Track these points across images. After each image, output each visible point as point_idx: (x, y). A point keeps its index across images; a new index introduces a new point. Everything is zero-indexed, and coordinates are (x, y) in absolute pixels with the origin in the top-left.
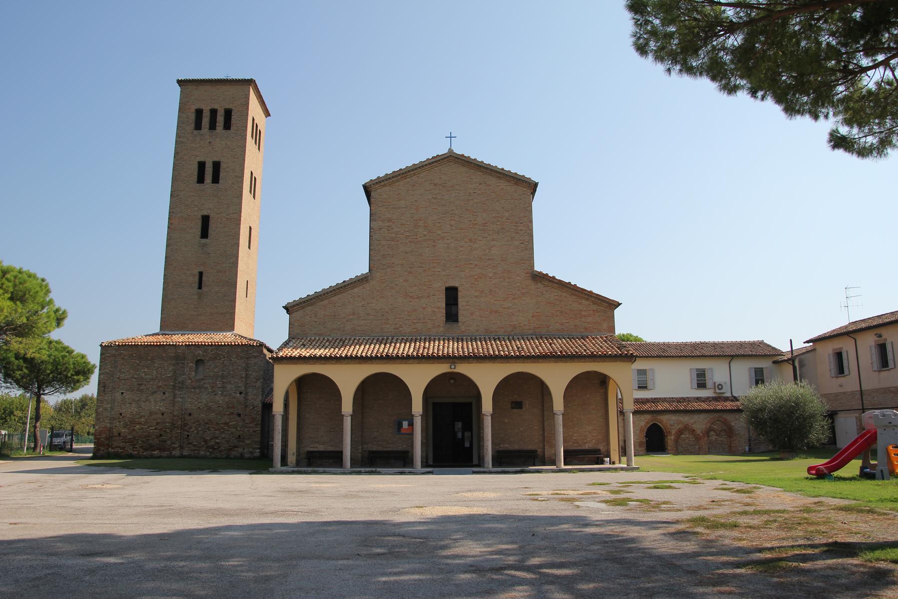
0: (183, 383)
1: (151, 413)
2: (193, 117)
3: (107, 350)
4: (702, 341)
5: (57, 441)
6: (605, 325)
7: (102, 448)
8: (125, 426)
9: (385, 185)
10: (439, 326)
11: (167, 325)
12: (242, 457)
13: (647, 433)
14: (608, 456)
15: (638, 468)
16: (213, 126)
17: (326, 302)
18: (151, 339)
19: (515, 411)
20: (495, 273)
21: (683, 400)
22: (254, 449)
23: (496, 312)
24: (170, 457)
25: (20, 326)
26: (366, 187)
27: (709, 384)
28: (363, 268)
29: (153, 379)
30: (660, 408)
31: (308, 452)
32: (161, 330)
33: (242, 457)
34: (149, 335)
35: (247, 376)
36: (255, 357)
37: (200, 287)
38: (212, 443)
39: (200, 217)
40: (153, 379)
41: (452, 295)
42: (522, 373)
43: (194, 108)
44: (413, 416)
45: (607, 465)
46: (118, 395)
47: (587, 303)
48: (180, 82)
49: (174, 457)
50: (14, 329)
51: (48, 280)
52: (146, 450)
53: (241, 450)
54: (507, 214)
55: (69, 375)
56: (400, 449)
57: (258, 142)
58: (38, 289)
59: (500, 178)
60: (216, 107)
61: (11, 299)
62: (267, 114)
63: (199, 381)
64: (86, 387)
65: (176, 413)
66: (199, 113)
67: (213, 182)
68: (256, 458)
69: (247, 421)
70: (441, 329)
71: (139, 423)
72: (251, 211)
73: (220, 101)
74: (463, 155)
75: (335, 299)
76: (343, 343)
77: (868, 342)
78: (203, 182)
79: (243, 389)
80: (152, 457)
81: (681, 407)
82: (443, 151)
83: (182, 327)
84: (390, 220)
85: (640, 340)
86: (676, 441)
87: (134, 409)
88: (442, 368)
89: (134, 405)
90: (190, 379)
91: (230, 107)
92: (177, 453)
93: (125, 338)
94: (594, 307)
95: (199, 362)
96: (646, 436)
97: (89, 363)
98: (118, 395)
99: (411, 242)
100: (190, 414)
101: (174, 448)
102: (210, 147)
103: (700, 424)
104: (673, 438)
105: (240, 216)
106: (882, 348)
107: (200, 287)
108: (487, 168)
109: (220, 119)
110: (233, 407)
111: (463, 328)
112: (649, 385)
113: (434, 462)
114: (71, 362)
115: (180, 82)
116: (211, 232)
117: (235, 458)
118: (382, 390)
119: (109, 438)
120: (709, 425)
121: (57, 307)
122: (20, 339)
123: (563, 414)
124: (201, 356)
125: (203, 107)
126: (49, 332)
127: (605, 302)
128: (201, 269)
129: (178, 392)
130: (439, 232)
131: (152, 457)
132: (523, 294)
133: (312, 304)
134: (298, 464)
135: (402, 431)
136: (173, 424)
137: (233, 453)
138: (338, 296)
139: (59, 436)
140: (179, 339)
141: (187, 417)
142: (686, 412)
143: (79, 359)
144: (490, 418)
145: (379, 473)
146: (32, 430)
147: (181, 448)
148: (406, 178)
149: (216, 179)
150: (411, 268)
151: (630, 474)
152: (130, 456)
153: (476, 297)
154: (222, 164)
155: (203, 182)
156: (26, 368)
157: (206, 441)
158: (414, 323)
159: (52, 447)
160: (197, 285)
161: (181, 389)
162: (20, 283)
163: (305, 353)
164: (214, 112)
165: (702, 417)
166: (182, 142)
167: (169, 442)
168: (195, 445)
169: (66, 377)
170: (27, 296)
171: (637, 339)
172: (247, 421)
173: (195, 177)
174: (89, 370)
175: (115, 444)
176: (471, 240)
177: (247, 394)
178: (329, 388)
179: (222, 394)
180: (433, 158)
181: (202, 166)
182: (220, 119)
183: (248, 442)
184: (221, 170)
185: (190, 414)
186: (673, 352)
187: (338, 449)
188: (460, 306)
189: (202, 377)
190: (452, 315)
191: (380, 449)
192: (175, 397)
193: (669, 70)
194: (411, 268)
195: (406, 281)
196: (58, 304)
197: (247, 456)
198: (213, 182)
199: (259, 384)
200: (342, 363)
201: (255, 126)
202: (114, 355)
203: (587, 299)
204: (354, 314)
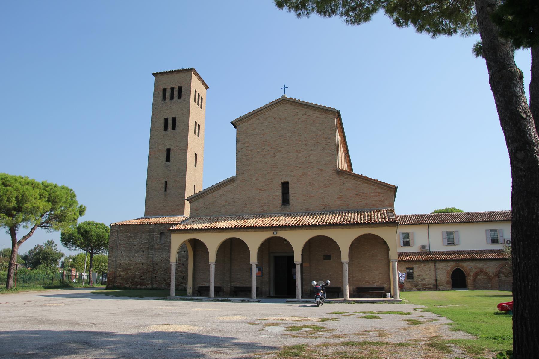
0: (153, 246)
1: (136, 264)
2: (161, 93)
3: (112, 226)
4: (497, 210)
6: (387, 202)
8: (123, 271)
9: (244, 122)
10: (277, 207)
11: (148, 213)
13: (452, 275)
14: (390, 292)
15: (401, 301)
16: (172, 98)
17: (210, 195)
18: (138, 221)
19: (326, 261)
20: (312, 172)
21: (481, 252)
23: (313, 197)
24: (146, 289)
27: (500, 240)
28: (231, 172)
29: (137, 244)
30: (462, 257)
31: (200, 287)
32: (146, 214)
37: (166, 190)
40: (137, 244)
41: (285, 186)
42: (317, 236)
43: (162, 88)
44: (251, 265)
45: (388, 299)
46: (119, 253)
48: (154, 74)
49: (148, 289)
52: (133, 285)
54: (320, 133)
55: (106, 242)
59: (315, 110)
62: (207, 87)
63: (161, 245)
65: (149, 264)
66: (165, 90)
70: (279, 209)
71: (130, 269)
74: (291, 98)
80: (137, 289)
81: (478, 257)
82: (278, 97)
84: (247, 143)
85: (462, 211)
86: (474, 280)
87: (127, 261)
89: (127, 259)
92: (149, 286)
94: (379, 190)
96: (452, 277)
98: (119, 253)
99: (260, 155)
100: (157, 264)
101: (148, 284)
102: (171, 110)
103: (491, 268)
104: (471, 278)
107: (166, 190)
108: (306, 105)
109: (176, 93)
111: (292, 208)
112: (456, 242)
115: (154, 74)
116: (171, 158)
118: (233, 248)
119: (115, 277)
120: (498, 269)
123: (348, 263)
127: (386, 186)
129: (150, 251)
130: (277, 148)
131: (137, 289)
132: (331, 184)
133: (202, 197)
134: (193, 294)
138: (218, 191)
140: (153, 220)
142: (480, 260)
144: (300, 266)
147: (152, 283)
148: (257, 116)
149: (174, 128)
150: (260, 171)
151: (396, 305)
152: (125, 288)
153: (300, 188)
157: (165, 280)
158: (262, 206)
160: (164, 189)
161: (152, 249)
163: (200, 226)
164: (172, 89)
165: (493, 263)
167: (145, 280)
168: (159, 282)
171: (458, 211)
175: (118, 281)
176: (297, 152)
180: (273, 101)
181: (166, 120)
182: (176, 93)
185: (157, 264)
186: (473, 219)
188: (290, 194)
190: (286, 200)
191: (242, 285)
193: (299, 14)
194: (260, 171)
195: (257, 180)
200: (209, 232)
202: (117, 231)
204: (226, 202)
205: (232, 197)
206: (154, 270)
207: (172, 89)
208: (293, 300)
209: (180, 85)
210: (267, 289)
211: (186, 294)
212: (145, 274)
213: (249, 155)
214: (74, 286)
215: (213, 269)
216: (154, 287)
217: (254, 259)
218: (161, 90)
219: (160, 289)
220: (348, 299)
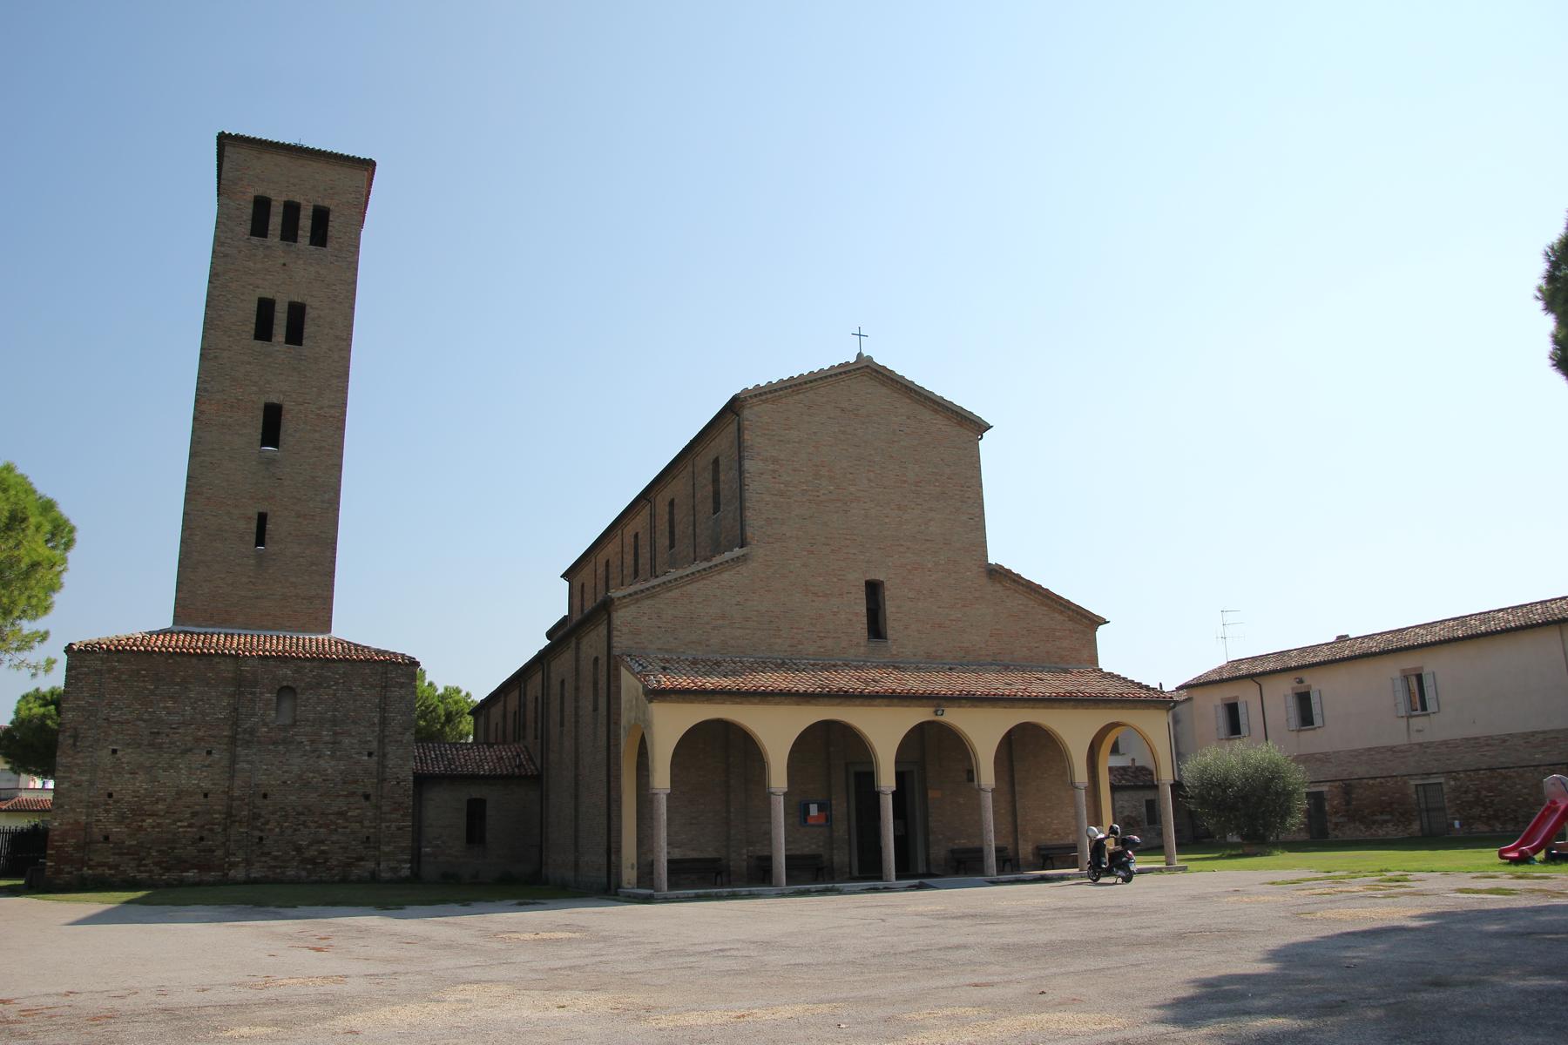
0: (252, 732)
1: (180, 794)
7: (68, 868)
8: (121, 818)
9: (764, 401)
12: (374, 878)
17: (675, 593)
22: (400, 862)
24: (225, 882)
32: (178, 617)
33: (374, 878)
35: (384, 722)
36: (402, 686)
37: (260, 540)
38: (312, 852)
39: (262, 406)
41: (874, 590)
46: (105, 753)
47: (1060, 618)
49: (236, 883)
52: (168, 869)
53: (371, 865)
56: (806, 851)
65: (237, 793)
70: (862, 649)
75: (690, 588)
76: (714, 667)
77: (1281, 694)
83: (223, 618)
84: (775, 461)
88: (920, 715)
89: (141, 776)
90: (265, 724)
91: (326, 203)
92: (238, 873)
94: (1070, 625)
95: (286, 691)
100: (265, 796)
102: (287, 274)
106: (1304, 700)
107: (260, 540)
110: (356, 782)
113: (860, 871)
117: (360, 881)
118: (831, 752)
124: (239, 675)
125: (270, 194)
128: (263, 507)
130: (852, 489)
131: (181, 883)
133: (653, 596)
135: (811, 822)
136: (229, 815)
138: (696, 585)
140: (237, 641)
141: (259, 802)
145: (840, 892)
147: (248, 863)
150: (812, 545)
154: (308, 310)
157: (298, 849)
166: (226, 256)
167: (219, 853)
168: (276, 858)
172: (385, 809)
177: (384, 755)
179: (332, 757)
180: (840, 365)
181: (265, 308)
185: (265, 796)
186: (613, 689)
187: (977, 844)
190: (876, 628)
192: (233, 760)
194: (812, 545)
195: (805, 565)
197: (386, 875)
200: (768, 703)
202: (99, 672)
203: (1062, 612)
204: (723, 617)
206: (256, 817)
208: (879, 884)
210: (846, 859)
212: (218, 829)
213: (782, 494)
215: (988, 800)
217: (778, 779)
220: (893, 881)
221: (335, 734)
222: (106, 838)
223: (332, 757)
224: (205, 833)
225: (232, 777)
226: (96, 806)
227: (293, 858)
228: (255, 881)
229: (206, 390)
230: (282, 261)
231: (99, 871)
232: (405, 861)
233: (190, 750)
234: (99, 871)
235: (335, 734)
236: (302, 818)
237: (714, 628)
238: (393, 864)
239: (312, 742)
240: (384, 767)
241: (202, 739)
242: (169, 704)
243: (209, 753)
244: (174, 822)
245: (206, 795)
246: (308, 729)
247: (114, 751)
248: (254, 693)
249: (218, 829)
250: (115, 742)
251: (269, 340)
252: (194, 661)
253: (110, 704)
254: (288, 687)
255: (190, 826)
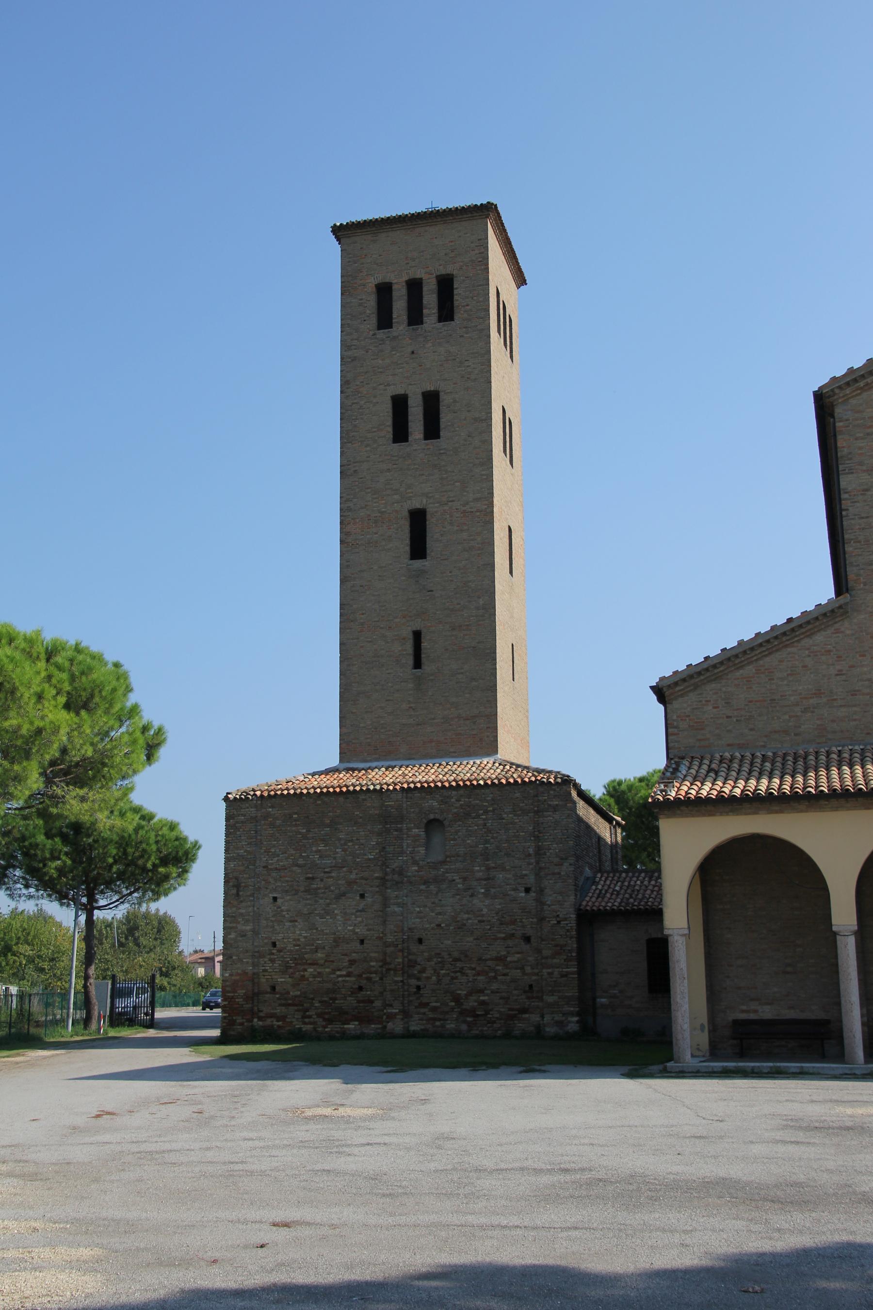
0: (401, 872)
1: (337, 941)
2: (371, 302)
5: (122, 1004)
7: (239, 1020)
8: (285, 969)
11: (354, 748)
12: (539, 1033)
16: (415, 317)
17: (749, 670)
24: (384, 1035)
25: (77, 764)
26: (824, 403)
32: (344, 755)
34: (320, 773)
35: (539, 852)
36: (555, 809)
37: (418, 664)
38: (471, 1003)
39: (406, 514)
44: (835, 934)
48: (339, 231)
49: (393, 1036)
50: (66, 773)
51: (127, 666)
52: (330, 1021)
53: (535, 1018)
55: (149, 865)
57: (508, 343)
58: (114, 683)
60: (419, 273)
61: (67, 706)
62: (520, 279)
64: (181, 889)
65: (390, 939)
66: (384, 291)
67: (426, 437)
68: (570, 1037)
69: (546, 953)
72: (512, 493)
73: (423, 261)
75: (769, 661)
76: (800, 762)
78: (405, 439)
79: (531, 880)
83: (387, 752)
90: (415, 863)
91: (449, 269)
93: (272, 780)
95: (433, 825)
97: (185, 839)
100: (420, 941)
101: (391, 1017)
102: (417, 361)
105: (491, 504)
107: (418, 664)
109: (430, 299)
110: (513, 922)
114: (152, 839)
115: (339, 231)
116: (431, 543)
119: (254, 996)
121: (144, 721)
122: (82, 792)
124: (436, 811)
125: (391, 278)
126: (135, 772)
131: (344, 1036)
136: (385, 963)
137: (519, 1026)
139: (128, 993)
143: (165, 831)
144: (852, 941)
146: (82, 982)
149: (432, 431)
154: (442, 396)
155: (405, 439)
156: (66, 854)
157: (457, 999)
159: (117, 1019)
160: (410, 661)
162: (83, 673)
164: (415, 287)
166: (354, 359)
167: (378, 1004)
168: (434, 1009)
169: (144, 869)
170: (97, 699)
172: (546, 953)
173: (388, 430)
174: (186, 853)
175: (266, 1010)
177: (541, 891)
178: (798, 871)
179: (486, 895)
181: (400, 404)
182: (430, 299)
183: (550, 999)
184: (443, 409)
185: (420, 941)
189: (440, 858)
192: (385, 903)
196: (151, 714)
197: (551, 1030)
198: (426, 437)
199: (567, 868)
200: (821, 809)
201: (502, 308)
204: (818, 693)
205: (840, 673)
207: (415, 287)
209: (443, 271)
211: (840, 1056)
212: (375, 977)
214: (41, 1031)
216: (414, 1027)
217: (844, 913)
218: (371, 287)
219: (438, 1036)
221: (488, 869)
222: (273, 988)
223: (486, 895)
224: (363, 982)
225: (384, 922)
226: (262, 956)
227: (453, 1009)
228: (413, 1035)
229: (349, 509)
230: (410, 350)
231: (268, 1022)
232: (572, 1014)
233: (343, 894)
234: (268, 1022)
235: (488, 869)
236: (459, 964)
237: (805, 710)
238: (558, 1017)
239: (465, 879)
240: (543, 904)
241: (355, 882)
242: (321, 847)
243: (362, 896)
244: (334, 971)
245: (362, 942)
246: (458, 865)
247: (275, 899)
248: (400, 830)
249: (375, 977)
250: (275, 890)
251: (406, 440)
252: (341, 799)
253: (267, 851)
254: (435, 820)
255: (349, 975)
